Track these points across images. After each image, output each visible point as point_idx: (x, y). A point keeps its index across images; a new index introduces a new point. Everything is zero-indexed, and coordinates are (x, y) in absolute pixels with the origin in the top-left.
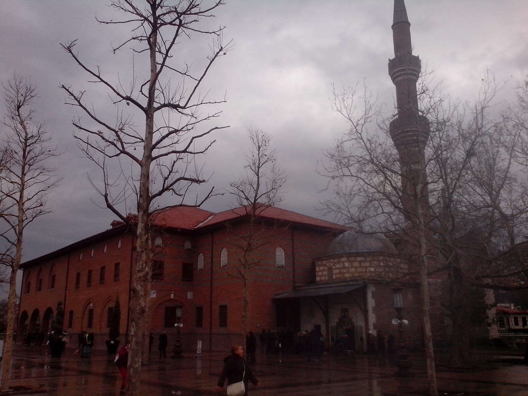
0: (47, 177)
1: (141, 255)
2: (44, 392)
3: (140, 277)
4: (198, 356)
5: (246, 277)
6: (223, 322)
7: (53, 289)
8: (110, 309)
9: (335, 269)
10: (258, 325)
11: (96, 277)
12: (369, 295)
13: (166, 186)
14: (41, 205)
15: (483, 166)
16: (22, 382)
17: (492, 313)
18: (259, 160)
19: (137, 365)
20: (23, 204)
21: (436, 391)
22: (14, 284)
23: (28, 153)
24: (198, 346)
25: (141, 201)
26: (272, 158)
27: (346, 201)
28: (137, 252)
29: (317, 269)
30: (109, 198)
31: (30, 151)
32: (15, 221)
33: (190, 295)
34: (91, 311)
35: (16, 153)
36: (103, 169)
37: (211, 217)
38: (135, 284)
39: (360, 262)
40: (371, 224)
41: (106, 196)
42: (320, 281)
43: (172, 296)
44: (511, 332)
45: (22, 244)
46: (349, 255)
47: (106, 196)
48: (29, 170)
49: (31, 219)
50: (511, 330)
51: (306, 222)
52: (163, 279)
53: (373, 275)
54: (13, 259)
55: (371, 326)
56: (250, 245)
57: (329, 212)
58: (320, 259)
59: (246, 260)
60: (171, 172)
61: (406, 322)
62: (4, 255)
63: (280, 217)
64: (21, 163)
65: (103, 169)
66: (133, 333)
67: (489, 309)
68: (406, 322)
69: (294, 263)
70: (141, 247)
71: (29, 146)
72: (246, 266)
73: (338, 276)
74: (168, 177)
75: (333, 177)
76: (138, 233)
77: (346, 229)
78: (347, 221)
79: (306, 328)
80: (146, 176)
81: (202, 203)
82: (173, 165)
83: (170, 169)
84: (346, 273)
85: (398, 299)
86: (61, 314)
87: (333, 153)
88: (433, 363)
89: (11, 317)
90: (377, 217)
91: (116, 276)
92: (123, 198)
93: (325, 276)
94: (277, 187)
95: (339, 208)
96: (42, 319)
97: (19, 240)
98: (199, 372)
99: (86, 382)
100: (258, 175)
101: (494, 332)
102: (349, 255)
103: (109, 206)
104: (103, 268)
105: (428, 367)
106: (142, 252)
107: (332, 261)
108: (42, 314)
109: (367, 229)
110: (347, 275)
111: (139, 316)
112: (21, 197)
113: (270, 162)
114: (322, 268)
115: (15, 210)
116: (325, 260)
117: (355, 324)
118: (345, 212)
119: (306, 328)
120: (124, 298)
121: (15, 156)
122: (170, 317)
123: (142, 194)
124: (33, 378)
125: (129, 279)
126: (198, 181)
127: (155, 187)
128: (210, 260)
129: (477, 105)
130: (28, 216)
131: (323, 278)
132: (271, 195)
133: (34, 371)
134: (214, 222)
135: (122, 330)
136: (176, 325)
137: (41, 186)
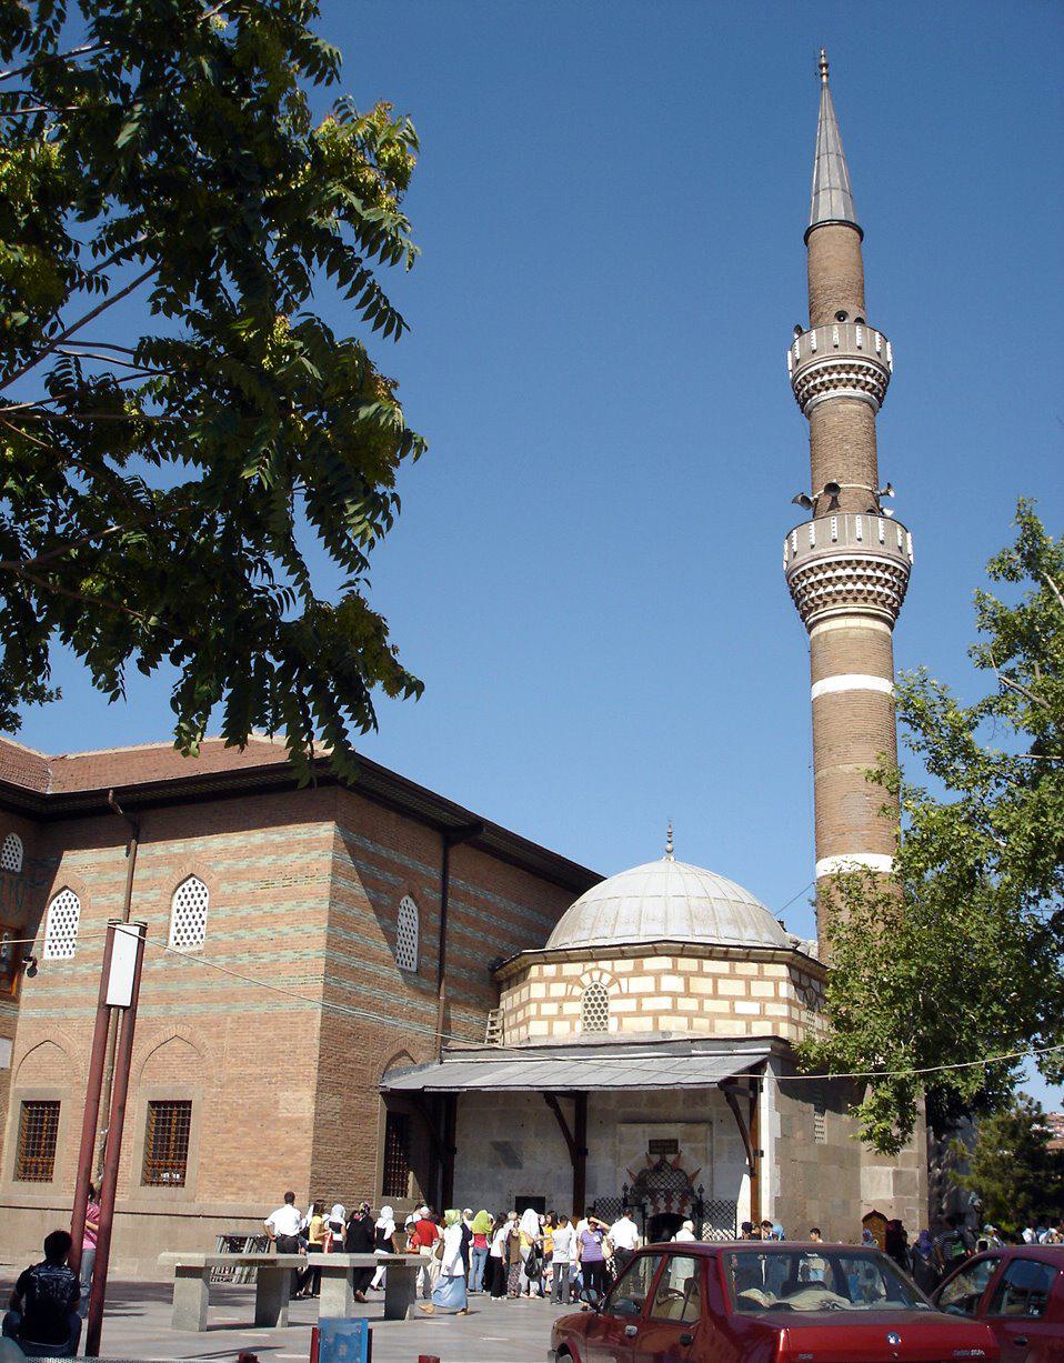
9: (615, 997)
93: (572, 1018)
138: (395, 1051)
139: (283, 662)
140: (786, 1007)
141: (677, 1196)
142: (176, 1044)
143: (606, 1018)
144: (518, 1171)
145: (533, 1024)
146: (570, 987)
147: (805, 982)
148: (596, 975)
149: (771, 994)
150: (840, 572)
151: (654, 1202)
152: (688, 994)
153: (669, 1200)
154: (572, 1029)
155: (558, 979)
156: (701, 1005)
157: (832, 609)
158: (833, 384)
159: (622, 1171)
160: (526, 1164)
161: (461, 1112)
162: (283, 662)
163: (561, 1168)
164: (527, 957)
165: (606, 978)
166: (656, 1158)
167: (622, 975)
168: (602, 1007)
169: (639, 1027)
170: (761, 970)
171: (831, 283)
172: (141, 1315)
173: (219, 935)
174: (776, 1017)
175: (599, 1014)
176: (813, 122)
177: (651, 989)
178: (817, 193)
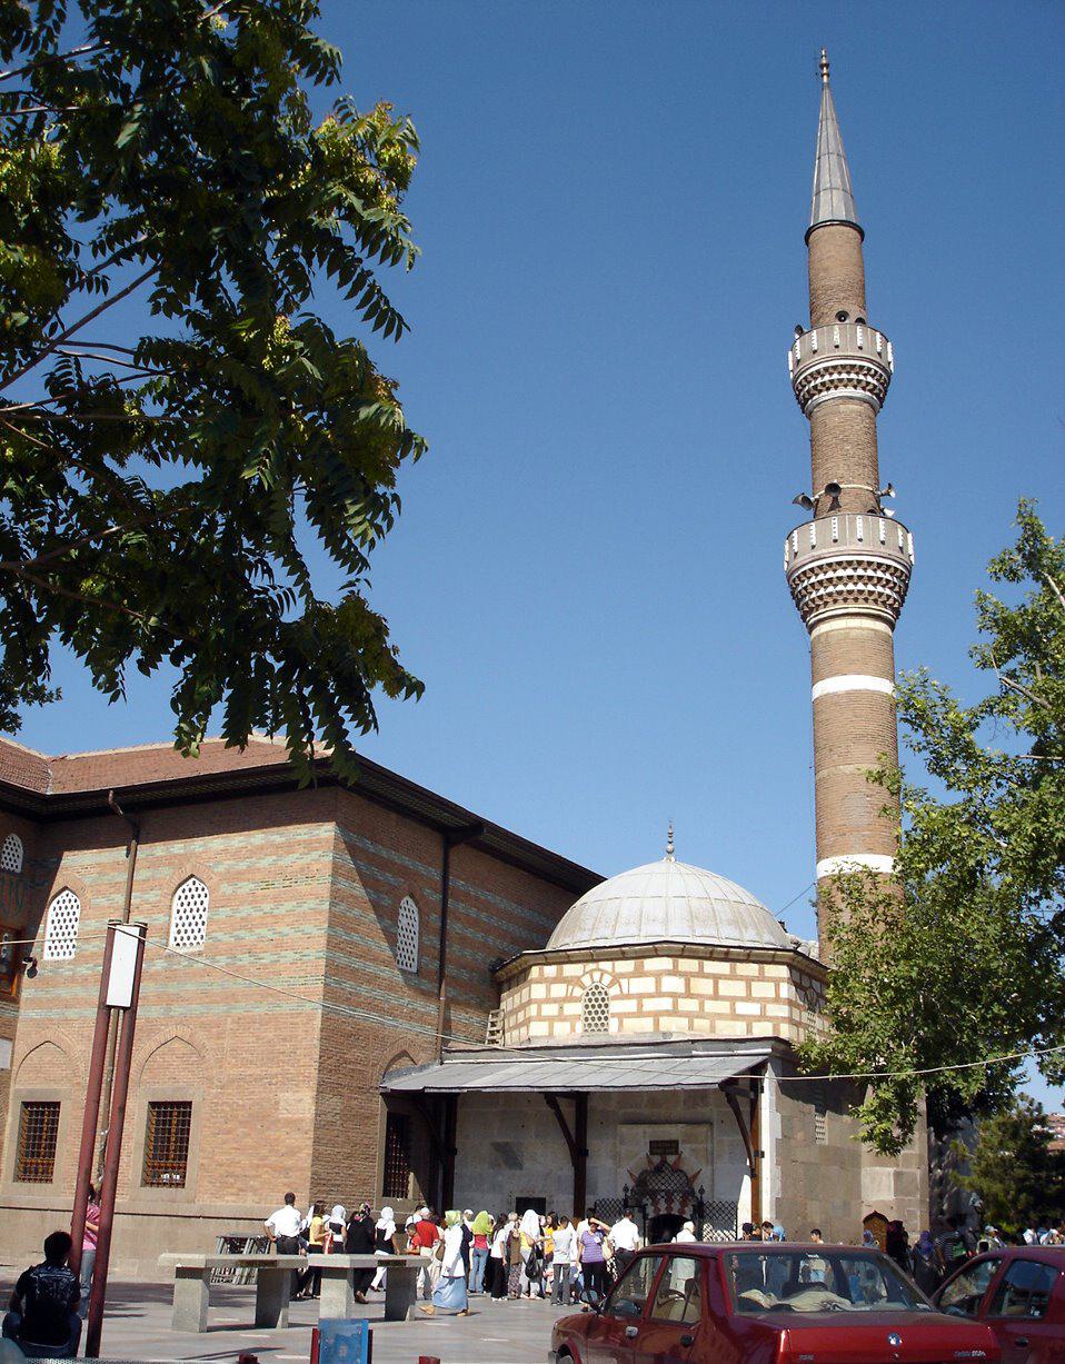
9: (616, 998)
93: (573, 1019)
138: (395, 1052)
139: (283, 662)
140: (787, 1007)
141: (678, 1197)
142: (176, 1044)
143: (606, 1018)
144: (518, 1172)
145: (533, 1025)
146: (570, 987)
147: (806, 983)
148: (597, 976)
149: (772, 994)
150: (841, 572)
151: (655, 1203)
152: (688, 995)
153: (669, 1201)
154: (573, 1029)
155: (558, 979)
156: (702, 1005)
157: (833, 609)
158: (834, 384)
159: (623, 1172)
160: (527, 1165)
161: (461, 1113)
162: (283, 662)
163: (561, 1169)
164: (527, 957)
165: (607, 979)
166: (656, 1159)
167: (623, 975)
168: (603, 1008)
169: (640, 1028)
170: (761, 971)
171: (832, 283)
172: (141, 1316)
173: (219, 935)
174: (777, 1018)
175: (600, 1015)
176: (814, 122)
177: (652, 989)
178: (818, 193)
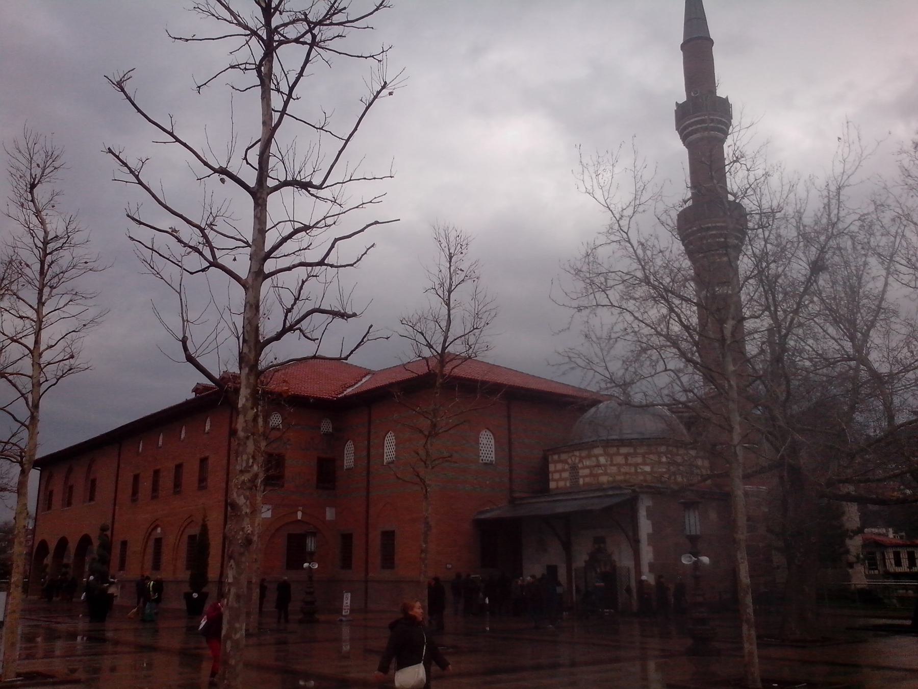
0: (83, 308)
1: (245, 444)
2: (77, 682)
3: (243, 482)
4: (344, 619)
5: (427, 482)
6: (388, 560)
7: (92, 503)
8: (192, 538)
9: (582, 468)
10: (449, 566)
11: (167, 481)
12: (642, 513)
13: (288, 324)
14: (72, 357)
15: (840, 289)
16: (38, 665)
17: (855, 544)
18: (451, 279)
19: (238, 636)
20: (40, 355)
21: (759, 680)
22: (25, 494)
23: (49, 266)
24: (345, 602)
25: (246, 350)
26: (473, 275)
27: (602, 350)
28: (239, 439)
29: (552, 467)
30: (189, 344)
31: (52, 262)
32: (25, 384)
33: (330, 514)
34: (158, 541)
35: (28, 266)
36: (180, 293)
37: (368, 377)
38: (235, 494)
39: (626, 456)
40: (644, 389)
41: (184, 341)
42: (557, 488)
43: (300, 515)
44: (888, 578)
45: (39, 424)
46: (607, 444)
47: (184, 341)
48: (50, 296)
49: (54, 381)
50: (888, 575)
51: (532, 387)
52: (283, 486)
53: (649, 478)
54: (22, 450)
55: (645, 568)
56: (434, 426)
57: (573, 368)
58: (556, 450)
59: (427, 452)
60: (296, 299)
61: (705, 559)
62: (6, 443)
63: (486, 378)
64: (37, 284)
65: (180, 293)
66: (230, 580)
67: (851, 538)
68: (705, 559)
69: (510, 457)
70: (245, 430)
71: (50, 253)
72: (428, 462)
73: (587, 480)
74: (292, 308)
75: (579, 309)
76: (240, 405)
77: (601, 399)
78: (603, 385)
79: (532, 571)
80: (253, 307)
81: (351, 353)
82: (301, 288)
83: (296, 294)
84: (602, 474)
85: (692, 521)
86: (106, 546)
87: (579, 265)
88: (753, 632)
89: (19, 551)
90: (656, 378)
91: (202, 480)
92: (214, 345)
93: (565, 480)
94: (482, 325)
95: (590, 362)
96: (72, 556)
97: (34, 418)
98: (346, 648)
99: (150, 665)
100: (448, 305)
101: (860, 578)
102: (607, 444)
103: (190, 359)
104: (179, 467)
105: (745, 639)
106: (248, 438)
107: (577, 453)
108: (72, 546)
109: (638, 398)
110: (604, 479)
111: (242, 550)
112: (37, 342)
113: (470, 281)
114: (559, 466)
115: (26, 365)
116: (565, 452)
117: (618, 564)
118: (600, 370)
119: (532, 571)
120: (215, 519)
121: (27, 271)
122: (296, 552)
123: (247, 338)
124: (58, 657)
125: (224, 485)
126: (343, 315)
127: (269, 326)
128: (365, 453)
129: (830, 183)
130: (49, 376)
131: (561, 484)
132: (472, 339)
133: (59, 646)
134: (372, 386)
135: (213, 574)
136: (306, 565)
137: (72, 324)
